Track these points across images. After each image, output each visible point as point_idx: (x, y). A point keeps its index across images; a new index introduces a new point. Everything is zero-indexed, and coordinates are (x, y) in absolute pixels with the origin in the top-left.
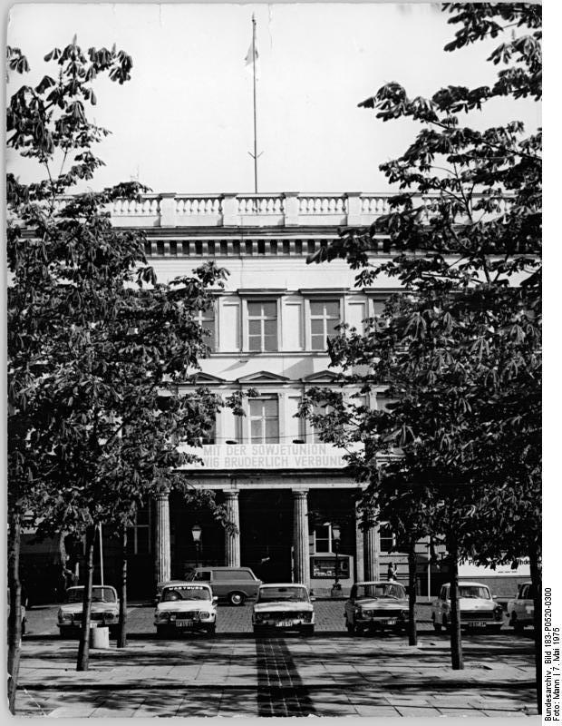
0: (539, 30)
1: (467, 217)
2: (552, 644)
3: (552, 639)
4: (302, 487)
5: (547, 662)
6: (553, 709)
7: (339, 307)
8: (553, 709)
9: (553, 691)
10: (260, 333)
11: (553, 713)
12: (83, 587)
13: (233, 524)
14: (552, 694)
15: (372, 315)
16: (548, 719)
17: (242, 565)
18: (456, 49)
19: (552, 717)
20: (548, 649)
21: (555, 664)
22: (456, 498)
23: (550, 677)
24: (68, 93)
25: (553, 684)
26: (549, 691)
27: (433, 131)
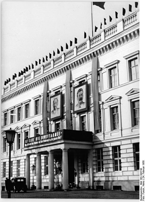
2: (142, 179)
3: (142, 178)
5: (141, 184)
6: (142, 197)
8: (142, 197)
10: (100, 166)
11: (142, 198)
12: (104, 189)
13: (65, 151)
16: (141, 200)
17: (113, 189)
19: (142, 199)
20: (141, 181)
21: (143, 175)
23: (142, 188)
24: (8, 178)
27: (116, 123)
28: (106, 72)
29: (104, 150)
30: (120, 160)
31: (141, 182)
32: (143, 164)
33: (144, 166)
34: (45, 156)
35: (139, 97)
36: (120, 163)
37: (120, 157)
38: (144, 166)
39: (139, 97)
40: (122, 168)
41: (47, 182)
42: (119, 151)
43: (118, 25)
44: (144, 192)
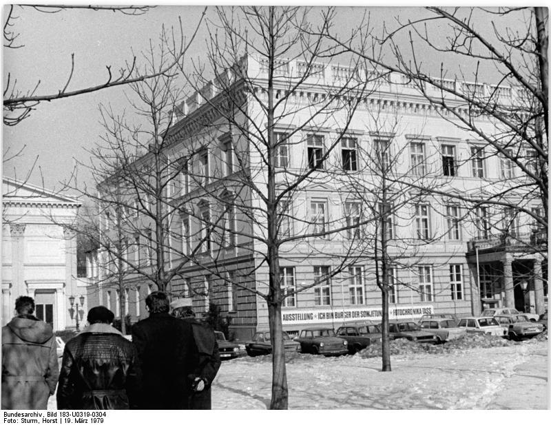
4: (288, 157)
5: (49, 414)
6: (13, 418)
8: (13, 418)
9: (27, 418)
11: (10, 418)
14: (24, 417)
15: (498, 109)
16: (5, 414)
19: (7, 417)
21: (72, 419)
23: (37, 416)
25: (33, 418)
26: (27, 415)
30: (452, 280)
34: (287, 273)
36: (451, 276)
37: (452, 285)
40: (62, 355)
41: (452, 16)
42: (457, 272)
44: (30, 421)
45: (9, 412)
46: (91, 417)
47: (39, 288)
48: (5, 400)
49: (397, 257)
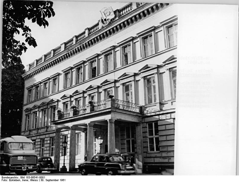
0: (140, 3)
1: (23, 131)
6: (6, 179)
7: (121, 142)
8: (6, 179)
11: (4, 179)
16: (2, 177)
18: (2, 60)
20: (25, 177)
22: (159, 168)
23: (16, 178)
25: (36, 179)
26: (12, 178)
28: (163, 31)
29: (159, 123)
31: (24, 178)
32: (63, 180)
33: (59, 181)
35: (177, 46)
38: (59, 181)
39: (177, 46)
43: (62, 46)
45: (4, 176)
46: (31, 178)
47: (157, 96)
48: (55, 158)
49: (131, 7)
